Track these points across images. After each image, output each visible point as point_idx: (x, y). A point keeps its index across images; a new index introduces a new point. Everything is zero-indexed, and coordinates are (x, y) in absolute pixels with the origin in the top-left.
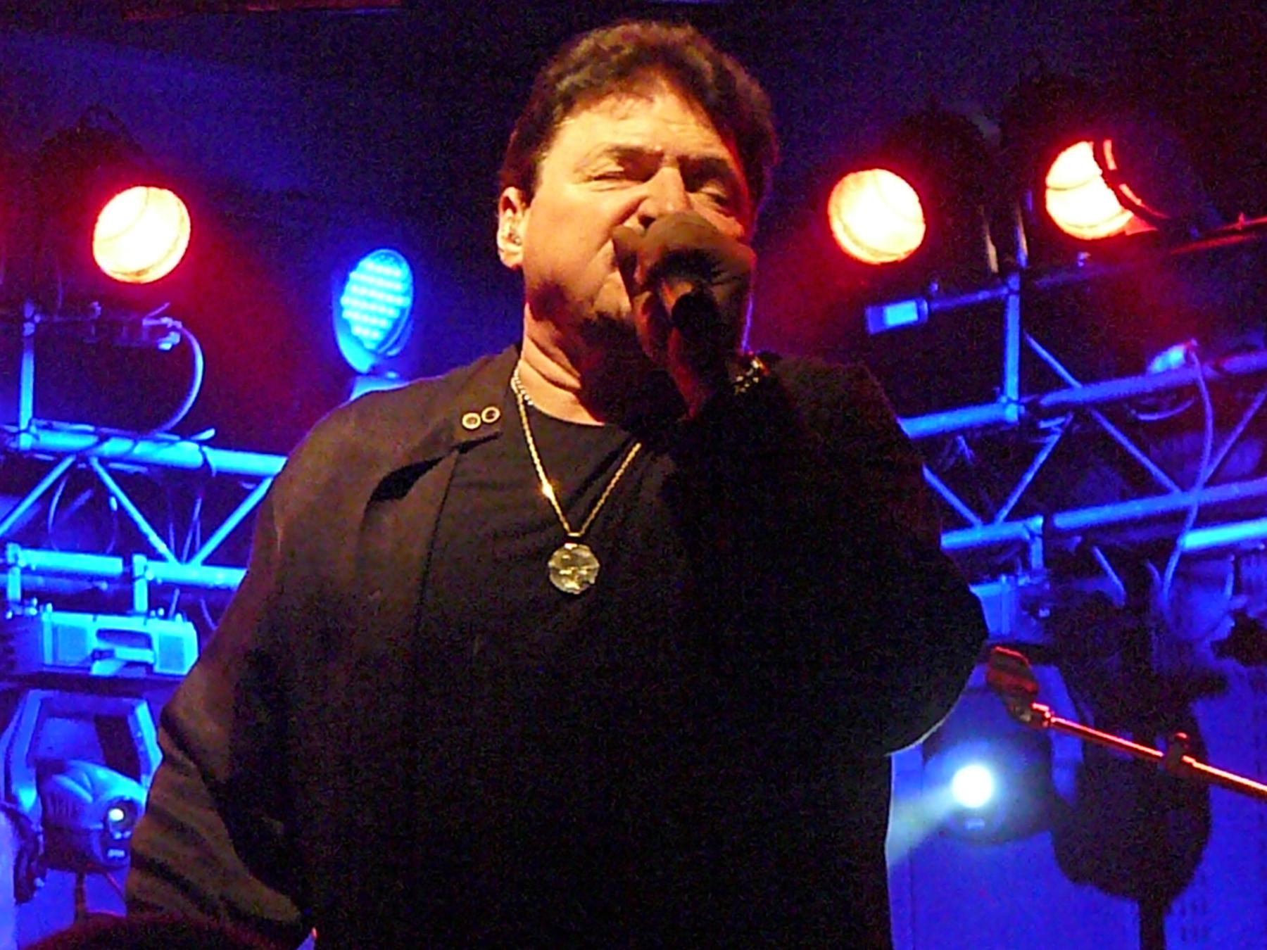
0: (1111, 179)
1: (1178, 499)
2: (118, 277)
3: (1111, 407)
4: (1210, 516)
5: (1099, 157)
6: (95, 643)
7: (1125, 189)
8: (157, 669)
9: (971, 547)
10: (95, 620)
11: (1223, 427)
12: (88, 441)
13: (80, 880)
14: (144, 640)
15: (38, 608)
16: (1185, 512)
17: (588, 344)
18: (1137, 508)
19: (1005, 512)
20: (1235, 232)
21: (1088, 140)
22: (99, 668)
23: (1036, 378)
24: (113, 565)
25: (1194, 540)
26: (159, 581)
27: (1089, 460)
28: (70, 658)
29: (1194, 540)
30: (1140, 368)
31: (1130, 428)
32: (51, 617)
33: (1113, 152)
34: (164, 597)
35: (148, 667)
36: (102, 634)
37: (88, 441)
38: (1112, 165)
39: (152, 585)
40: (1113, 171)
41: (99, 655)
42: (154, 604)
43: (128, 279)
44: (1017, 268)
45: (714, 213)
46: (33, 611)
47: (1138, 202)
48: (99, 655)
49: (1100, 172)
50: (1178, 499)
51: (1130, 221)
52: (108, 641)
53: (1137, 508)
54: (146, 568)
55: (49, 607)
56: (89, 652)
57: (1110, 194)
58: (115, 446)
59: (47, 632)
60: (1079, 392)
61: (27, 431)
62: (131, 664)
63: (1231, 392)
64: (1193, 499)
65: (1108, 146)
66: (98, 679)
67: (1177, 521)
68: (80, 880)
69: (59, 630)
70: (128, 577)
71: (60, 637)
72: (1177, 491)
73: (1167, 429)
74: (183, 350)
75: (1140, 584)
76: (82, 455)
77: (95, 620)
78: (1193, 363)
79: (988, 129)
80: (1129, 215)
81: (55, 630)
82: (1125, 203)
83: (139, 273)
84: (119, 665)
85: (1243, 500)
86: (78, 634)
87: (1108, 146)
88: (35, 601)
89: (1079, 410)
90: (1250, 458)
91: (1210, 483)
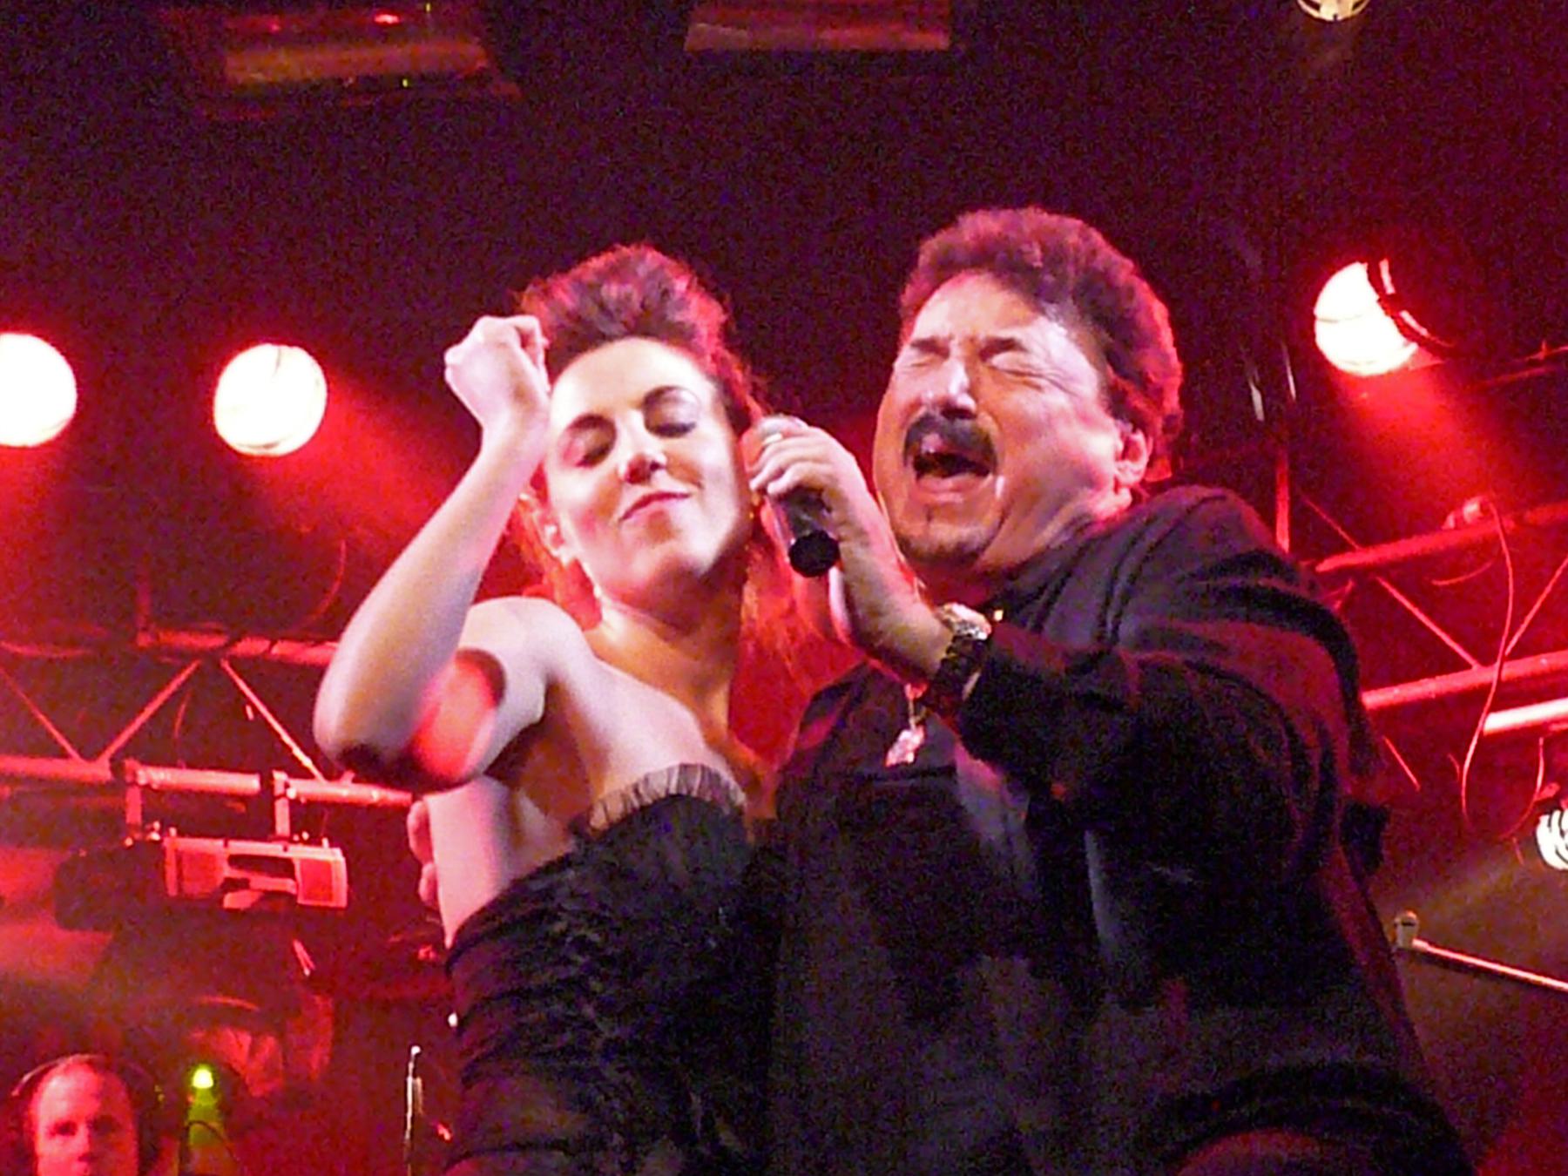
0: (1390, 305)
1: (1480, 675)
2: (244, 450)
4: (1512, 695)
5: (1375, 279)
6: (228, 872)
8: (300, 901)
9: (672, 694)
10: (226, 845)
12: (218, 641)
13: (577, 826)
14: (284, 867)
15: (160, 832)
16: (1485, 688)
18: (1429, 687)
19: (1493, 690)
20: (1536, 363)
21: (1362, 262)
22: (229, 900)
24: (252, 783)
25: (1496, 722)
26: (303, 800)
29: (1496, 722)
30: (1436, 524)
33: (1391, 272)
34: (314, 820)
35: (292, 898)
36: (235, 860)
37: (218, 641)
38: (1390, 290)
39: (294, 804)
40: (1392, 296)
41: (231, 885)
42: (295, 828)
43: (255, 452)
46: (155, 836)
47: (1424, 332)
48: (231, 885)
49: (1374, 297)
50: (1480, 675)
51: (1414, 356)
52: (240, 868)
53: (1429, 687)
54: (287, 786)
55: (173, 831)
56: (220, 881)
57: (1388, 324)
58: (251, 646)
59: (170, 858)
61: (145, 630)
62: (269, 895)
64: (1489, 675)
65: (1384, 267)
66: (233, 912)
67: (1475, 702)
68: (577, 826)
69: (185, 858)
70: (268, 793)
71: (185, 863)
72: (1476, 667)
75: (1440, 776)
76: (212, 656)
77: (226, 845)
78: (1492, 516)
80: (1414, 347)
81: (179, 857)
82: (1404, 329)
83: (268, 446)
84: (256, 895)
85: (1534, 677)
86: (208, 859)
87: (1384, 267)
88: (157, 825)
91: (1519, 653)
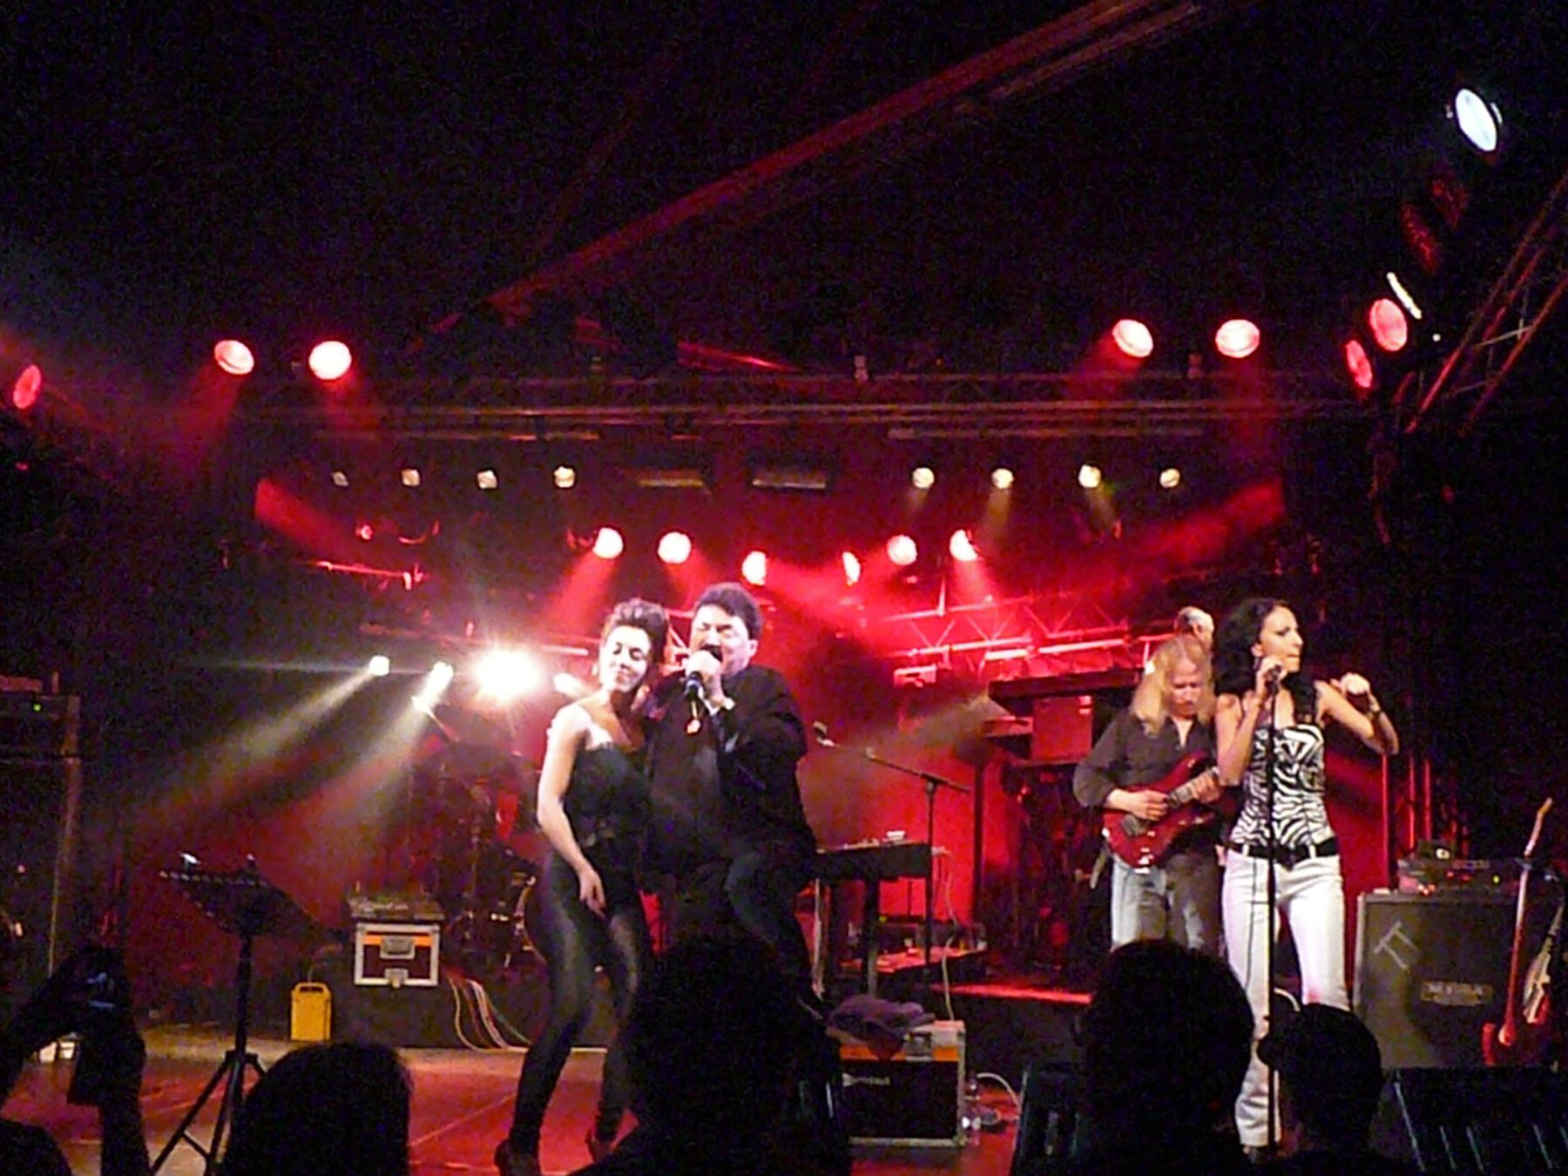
4: (994, 649)
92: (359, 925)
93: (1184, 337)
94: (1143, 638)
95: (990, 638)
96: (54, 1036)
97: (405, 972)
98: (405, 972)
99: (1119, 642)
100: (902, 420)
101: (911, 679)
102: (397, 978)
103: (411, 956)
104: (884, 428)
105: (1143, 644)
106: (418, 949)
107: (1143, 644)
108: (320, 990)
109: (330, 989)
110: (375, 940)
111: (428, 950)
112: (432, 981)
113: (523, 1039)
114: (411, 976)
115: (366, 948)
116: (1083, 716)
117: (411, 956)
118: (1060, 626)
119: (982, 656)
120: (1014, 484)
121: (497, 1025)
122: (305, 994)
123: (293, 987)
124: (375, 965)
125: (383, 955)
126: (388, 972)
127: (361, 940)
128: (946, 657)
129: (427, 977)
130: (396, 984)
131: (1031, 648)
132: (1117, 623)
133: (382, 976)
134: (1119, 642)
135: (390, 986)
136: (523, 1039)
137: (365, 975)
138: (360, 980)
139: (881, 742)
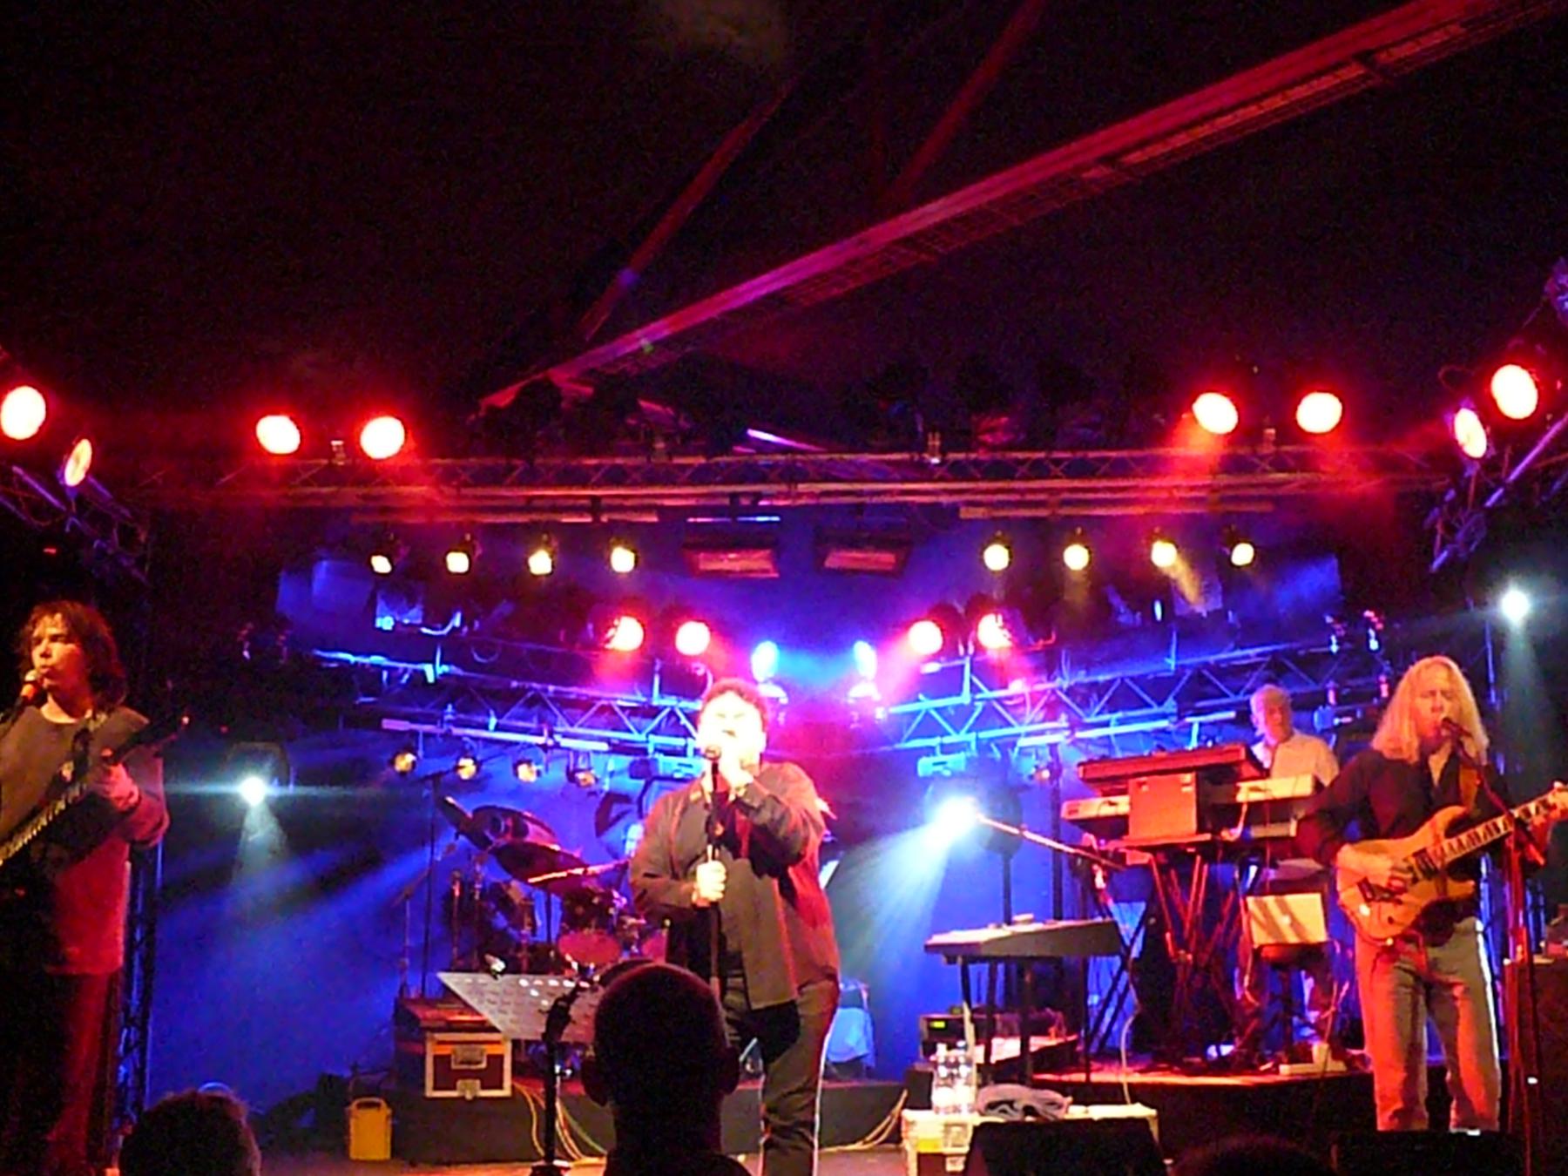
3: (999, 700)
4: (1028, 734)
7: (334, 665)
11: (1033, 705)
17: (330, 1077)
23: (974, 689)
27: (990, 716)
28: (669, 772)
31: (1004, 706)
32: (661, 757)
44: (1470, 763)
45: (17, 724)
60: (987, 694)
63: (1035, 697)
73: (1016, 706)
74: (705, 676)
75: (1005, 755)
79: (961, 610)
89: (987, 700)
90: (1041, 715)
92: (428, 1034)
93: (1267, 409)
94: (1189, 720)
95: (1021, 724)
96: (953, 1173)
97: (478, 1082)
98: (478, 1082)
99: (1163, 724)
100: (968, 497)
101: (939, 768)
102: (470, 1090)
103: (483, 1065)
104: (955, 508)
105: (1191, 725)
106: (490, 1057)
107: (1191, 725)
108: (377, 1105)
109: (389, 1104)
110: (445, 1050)
111: (501, 1057)
112: (506, 1092)
113: (600, 1149)
114: (484, 1087)
115: (436, 1058)
116: (1186, 794)
117: (483, 1065)
118: (1097, 710)
119: (1014, 745)
120: (1091, 567)
121: (574, 1136)
122: (362, 1111)
123: (349, 1104)
124: (446, 1076)
125: (454, 1066)
126: (459, 1083)
127: (431, 1051)
128: (973, 746)
129: (500, 1087)
130: (469, 1096)
131: (1067, 733)
132: (1160, 704)
133: (454, 1088)
134: (1163, 724)
135: (463, 1098)
136: (600, 1149)
137: (436, 1088)
138: (430, 1093)
139: (274, 852)
